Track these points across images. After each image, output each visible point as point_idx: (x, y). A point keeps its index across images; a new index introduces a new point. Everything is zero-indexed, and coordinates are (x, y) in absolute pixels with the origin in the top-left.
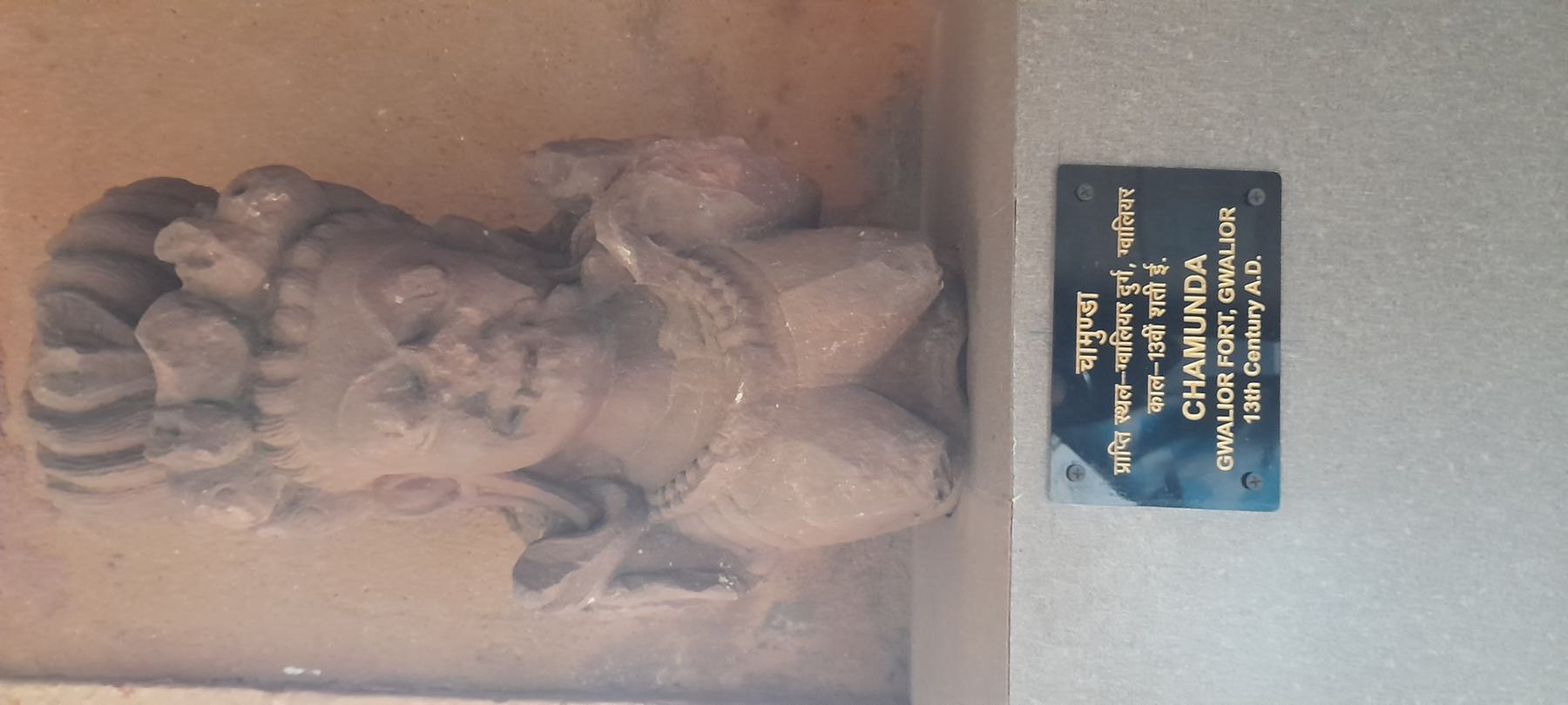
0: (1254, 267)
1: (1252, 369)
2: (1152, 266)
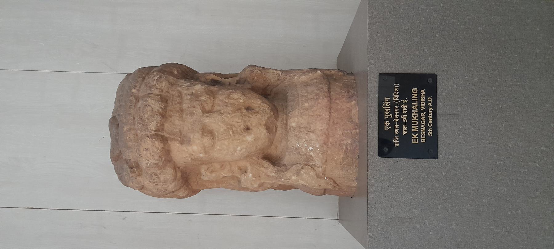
0: (430, 99)
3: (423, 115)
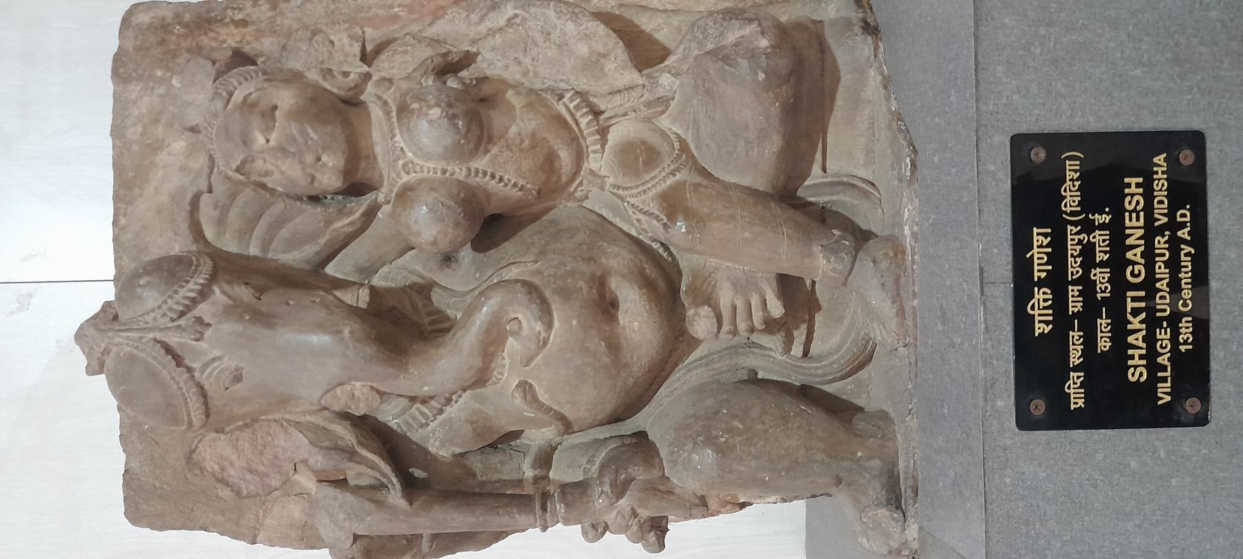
3: (1161, 242)
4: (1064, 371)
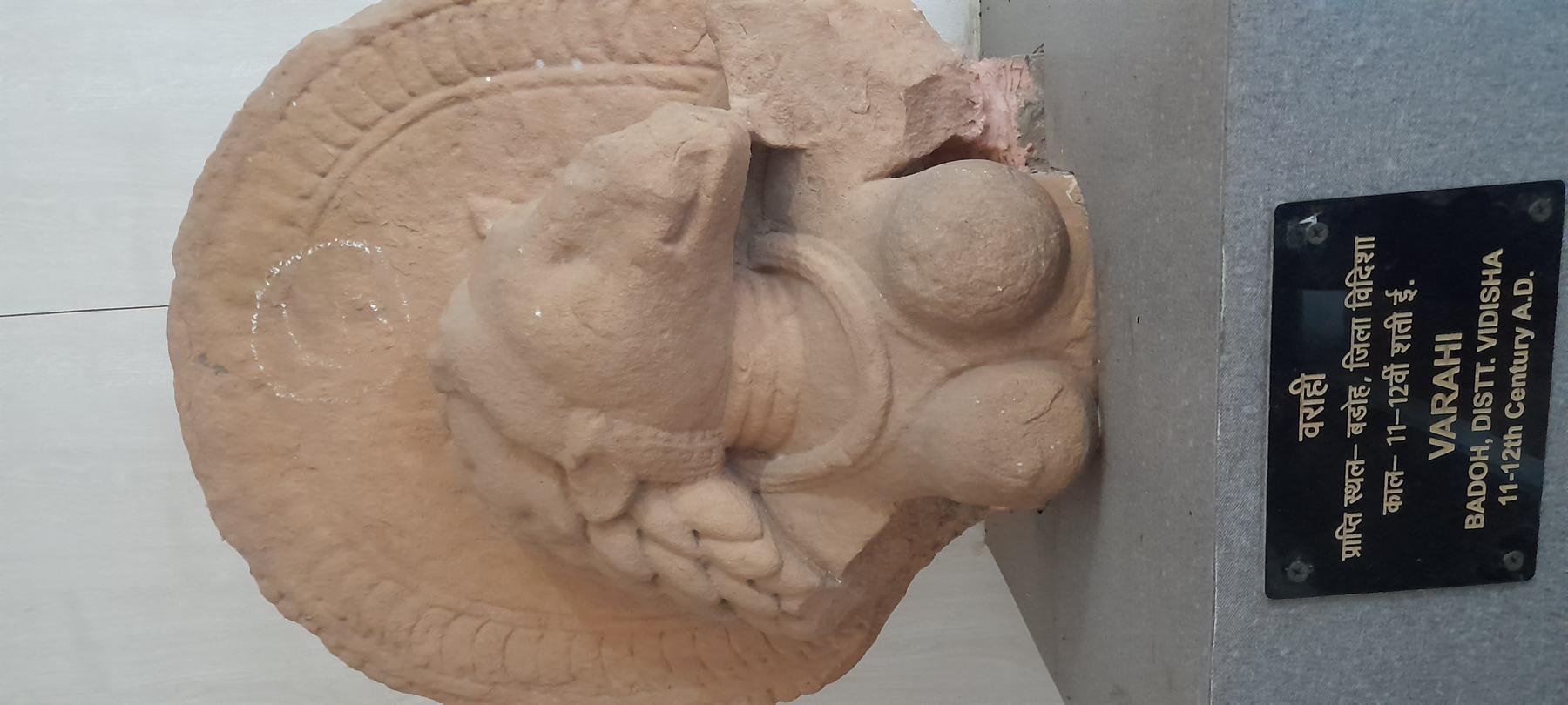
0: (1525, 287)
1: (1515, 409)
2: (1396, 293)
4: (1335, 512)
